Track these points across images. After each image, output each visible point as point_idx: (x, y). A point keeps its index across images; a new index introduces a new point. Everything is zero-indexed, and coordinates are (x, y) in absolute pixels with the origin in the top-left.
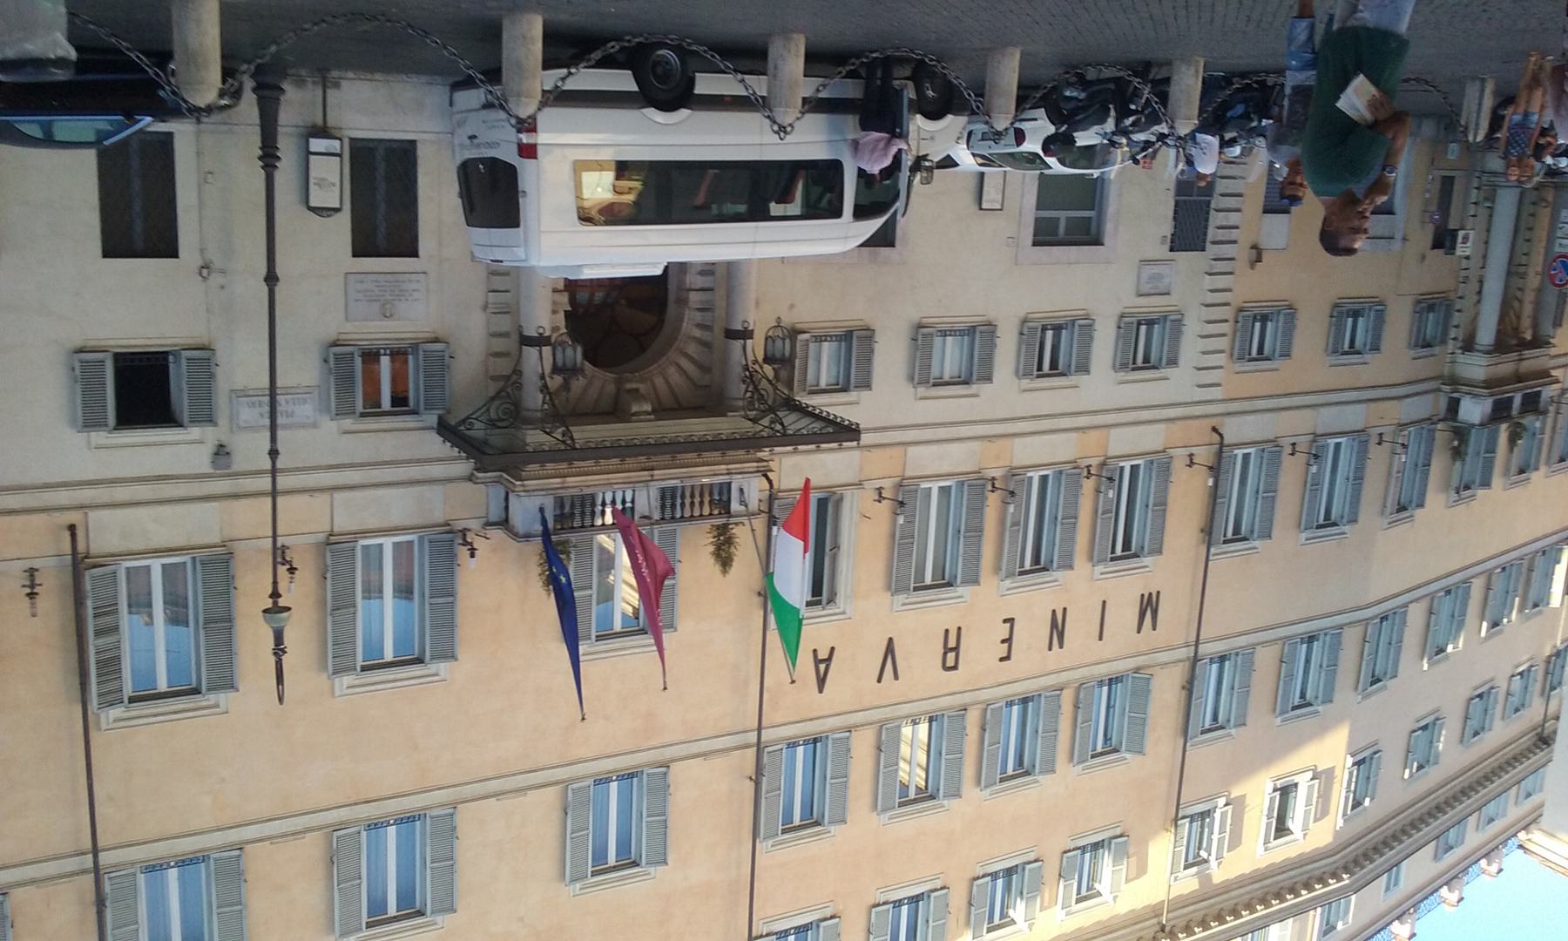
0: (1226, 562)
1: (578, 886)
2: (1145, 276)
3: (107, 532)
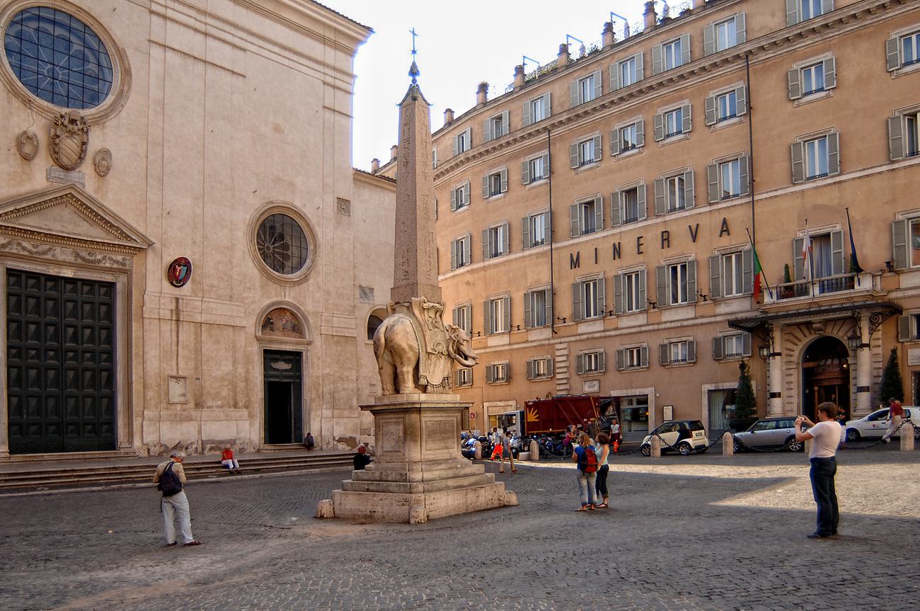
1: (832, 132)
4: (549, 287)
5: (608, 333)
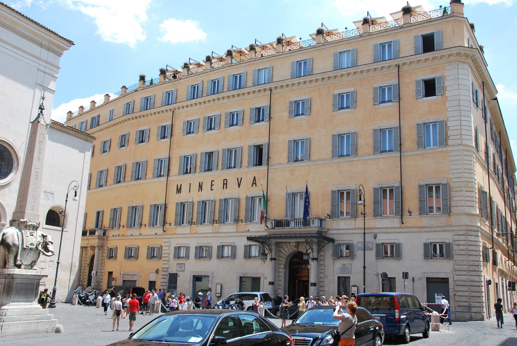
0: (161, 201)
2: (183, 268)
3: (396, 222)
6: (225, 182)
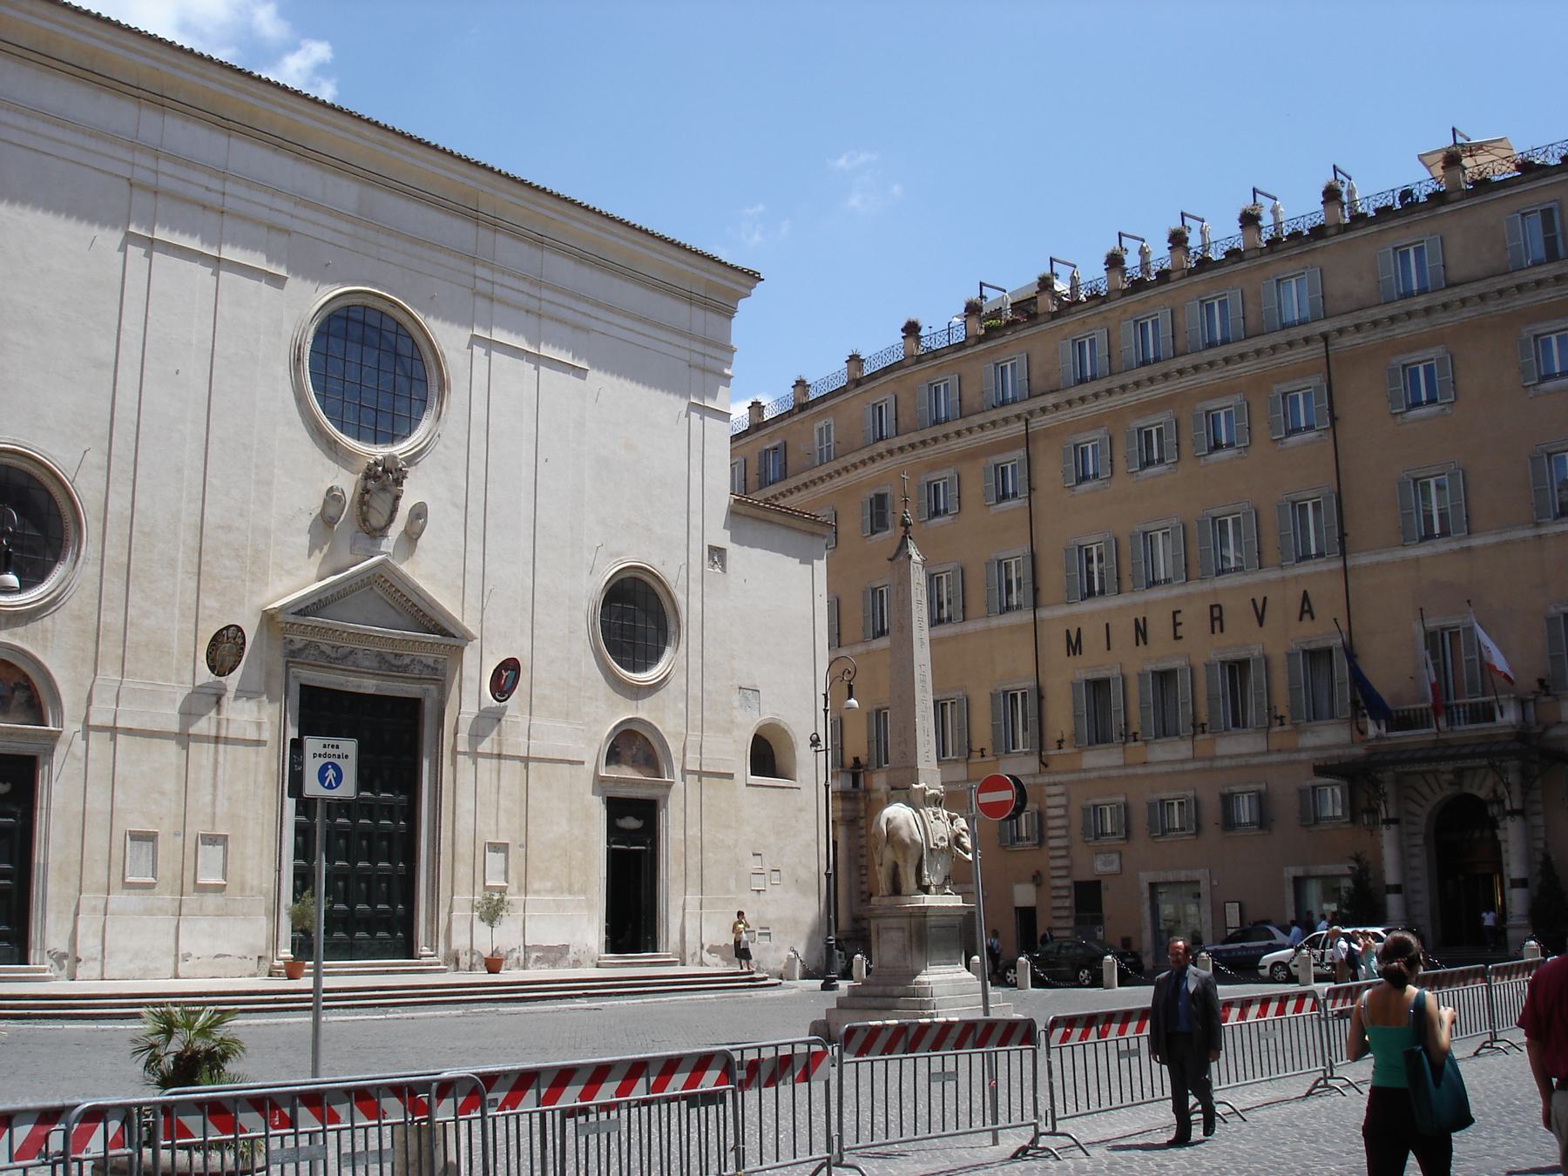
4: (1033, 684)
5: (1130, 771)
6: (1216, 614)
